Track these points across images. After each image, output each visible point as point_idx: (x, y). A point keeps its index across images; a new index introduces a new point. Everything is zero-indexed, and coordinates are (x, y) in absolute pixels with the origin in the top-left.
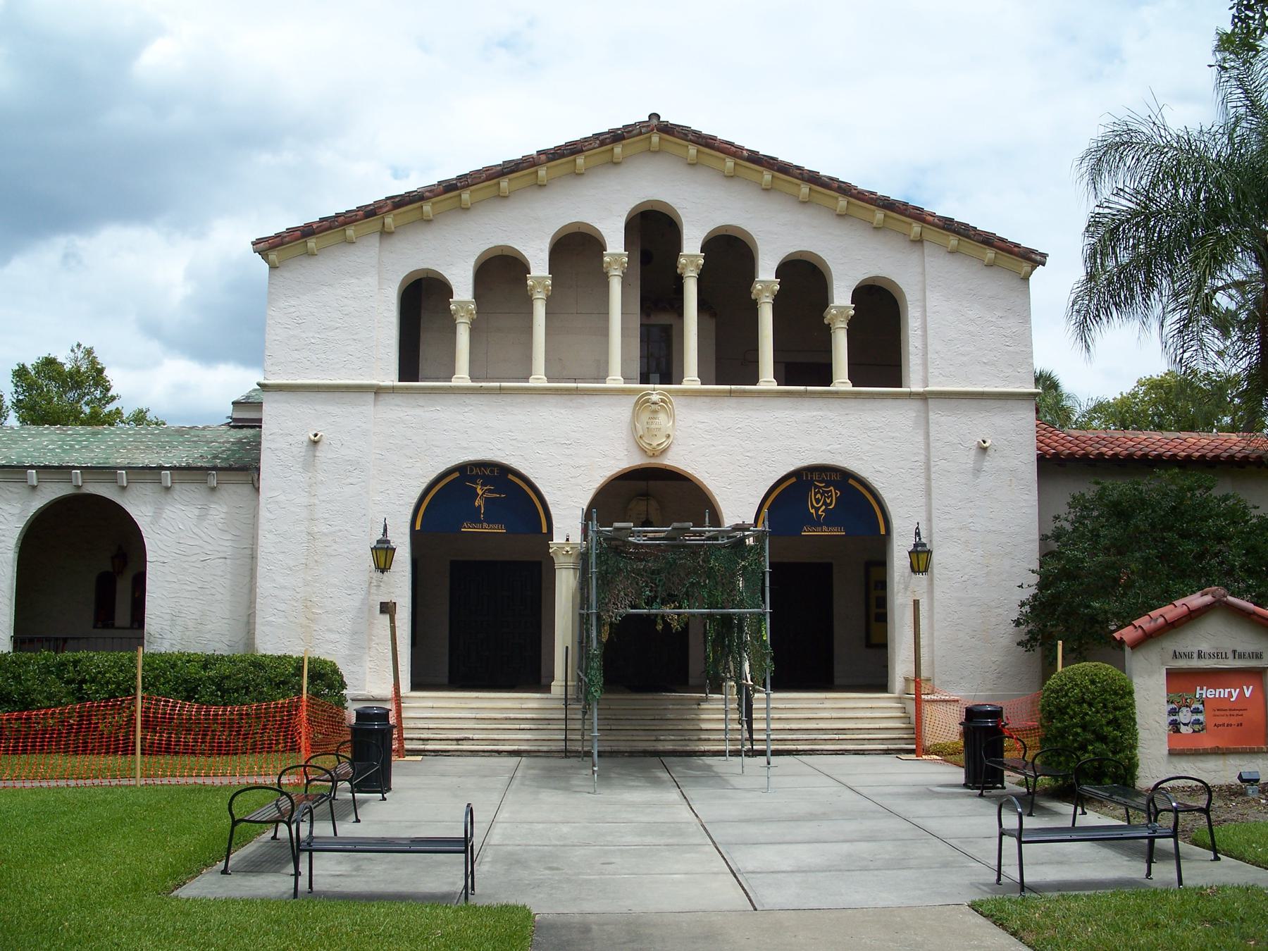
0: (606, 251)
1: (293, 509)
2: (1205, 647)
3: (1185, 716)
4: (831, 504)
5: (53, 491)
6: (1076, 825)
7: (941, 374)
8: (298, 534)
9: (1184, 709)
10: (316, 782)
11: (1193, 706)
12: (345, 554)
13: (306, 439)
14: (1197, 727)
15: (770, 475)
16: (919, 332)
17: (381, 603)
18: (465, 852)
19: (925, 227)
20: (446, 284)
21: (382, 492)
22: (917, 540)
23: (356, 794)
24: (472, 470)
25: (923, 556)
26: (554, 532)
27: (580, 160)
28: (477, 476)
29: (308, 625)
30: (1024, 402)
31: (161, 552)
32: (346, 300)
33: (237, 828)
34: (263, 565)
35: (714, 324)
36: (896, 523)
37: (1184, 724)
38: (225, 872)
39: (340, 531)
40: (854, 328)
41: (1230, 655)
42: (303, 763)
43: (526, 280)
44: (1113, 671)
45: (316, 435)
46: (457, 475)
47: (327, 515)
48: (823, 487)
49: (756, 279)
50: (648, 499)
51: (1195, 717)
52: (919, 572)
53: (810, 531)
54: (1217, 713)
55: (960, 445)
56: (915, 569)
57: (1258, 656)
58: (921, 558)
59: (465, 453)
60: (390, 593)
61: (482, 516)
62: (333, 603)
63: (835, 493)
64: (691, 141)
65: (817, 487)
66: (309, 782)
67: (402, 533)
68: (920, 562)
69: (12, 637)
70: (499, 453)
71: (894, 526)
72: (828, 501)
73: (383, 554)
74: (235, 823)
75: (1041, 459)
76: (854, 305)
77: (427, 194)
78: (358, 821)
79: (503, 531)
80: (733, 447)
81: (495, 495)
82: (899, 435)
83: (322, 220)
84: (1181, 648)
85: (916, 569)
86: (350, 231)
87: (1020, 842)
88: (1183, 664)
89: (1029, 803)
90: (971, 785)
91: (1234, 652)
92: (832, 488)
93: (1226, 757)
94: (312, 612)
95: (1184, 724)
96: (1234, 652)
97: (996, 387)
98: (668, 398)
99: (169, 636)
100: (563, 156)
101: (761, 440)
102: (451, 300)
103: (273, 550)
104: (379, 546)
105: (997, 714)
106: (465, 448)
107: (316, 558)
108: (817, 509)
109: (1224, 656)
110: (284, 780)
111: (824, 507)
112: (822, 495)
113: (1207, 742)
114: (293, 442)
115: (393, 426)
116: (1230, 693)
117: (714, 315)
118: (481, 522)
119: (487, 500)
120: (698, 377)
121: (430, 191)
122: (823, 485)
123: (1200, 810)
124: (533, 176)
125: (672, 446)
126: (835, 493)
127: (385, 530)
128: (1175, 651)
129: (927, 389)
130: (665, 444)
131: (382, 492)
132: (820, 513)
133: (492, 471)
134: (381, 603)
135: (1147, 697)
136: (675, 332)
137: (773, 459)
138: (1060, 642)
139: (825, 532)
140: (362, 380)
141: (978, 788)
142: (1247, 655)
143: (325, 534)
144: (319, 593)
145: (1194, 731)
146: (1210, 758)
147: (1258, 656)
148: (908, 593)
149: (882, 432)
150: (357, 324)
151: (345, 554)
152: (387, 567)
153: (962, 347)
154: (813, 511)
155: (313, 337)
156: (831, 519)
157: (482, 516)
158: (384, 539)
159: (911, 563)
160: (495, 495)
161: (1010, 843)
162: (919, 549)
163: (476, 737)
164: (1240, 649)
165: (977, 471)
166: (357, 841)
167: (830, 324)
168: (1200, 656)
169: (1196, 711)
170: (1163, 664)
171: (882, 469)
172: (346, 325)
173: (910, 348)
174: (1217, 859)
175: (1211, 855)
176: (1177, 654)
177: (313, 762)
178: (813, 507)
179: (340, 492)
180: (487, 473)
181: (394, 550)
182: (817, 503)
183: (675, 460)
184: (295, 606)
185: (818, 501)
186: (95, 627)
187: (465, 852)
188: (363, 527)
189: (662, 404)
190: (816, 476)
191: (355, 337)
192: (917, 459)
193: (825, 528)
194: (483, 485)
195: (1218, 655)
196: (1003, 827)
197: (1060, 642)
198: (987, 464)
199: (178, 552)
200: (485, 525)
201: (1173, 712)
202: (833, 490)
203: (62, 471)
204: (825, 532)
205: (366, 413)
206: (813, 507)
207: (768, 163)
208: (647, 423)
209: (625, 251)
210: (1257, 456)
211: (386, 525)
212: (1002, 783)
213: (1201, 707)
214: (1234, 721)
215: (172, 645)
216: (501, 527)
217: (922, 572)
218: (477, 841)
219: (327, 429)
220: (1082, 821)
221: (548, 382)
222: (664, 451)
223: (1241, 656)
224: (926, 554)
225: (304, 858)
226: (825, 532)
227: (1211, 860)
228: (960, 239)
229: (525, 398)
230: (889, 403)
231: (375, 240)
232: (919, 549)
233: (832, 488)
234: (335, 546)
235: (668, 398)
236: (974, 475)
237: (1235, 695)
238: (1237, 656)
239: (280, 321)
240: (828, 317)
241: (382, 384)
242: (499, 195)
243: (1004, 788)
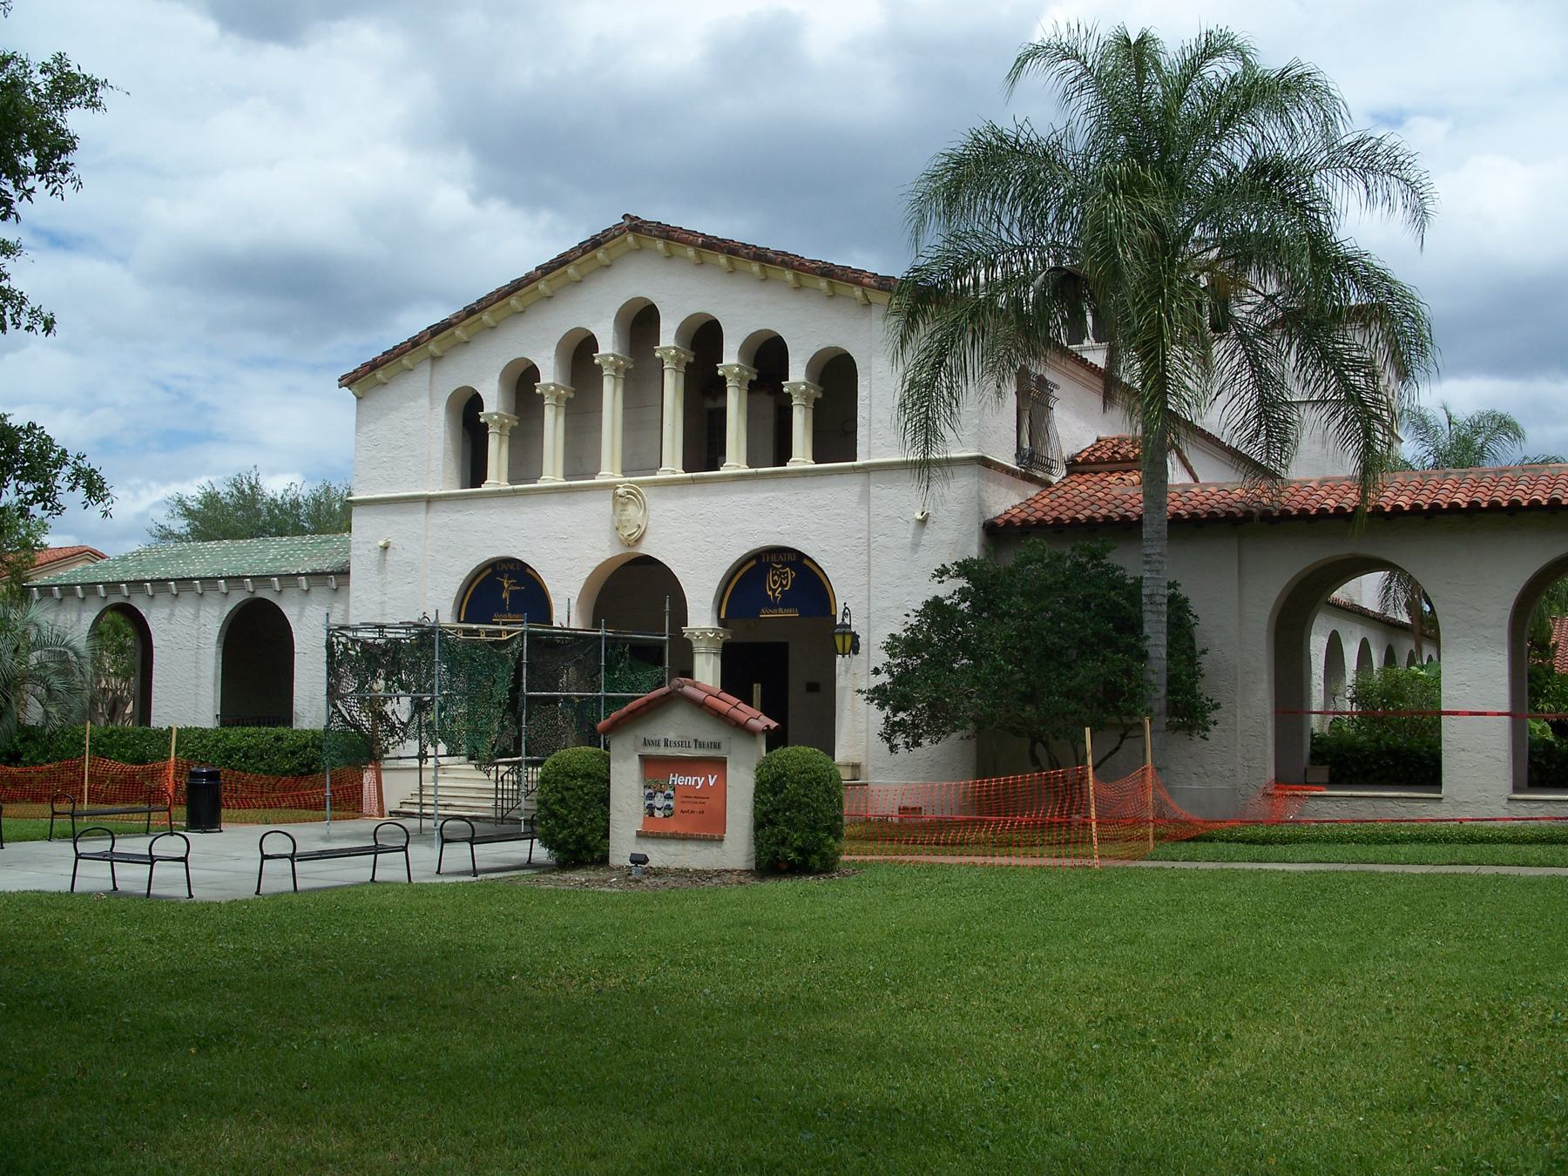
2: (671, 736)
3: (659, 801)
4: (786, 586)
5: (238, 597)
9: (659, 794)
11: (666, 792)
14: (668, 812)
16: (867, 402)
27: (571, 270)
28: (504, 572)
30: (966, 468)
31: (305, 646)
37: (659, 809)
41: (693, 744)
44: (821, 755)
46: (489, 571)
51: (667, 802)
54: (685, 800)
57: (717, 746)
63: (791, 574)
64: (655, 236)
72: (784, 583)
77: (455, 320)
83: (384, 353)
86: (405, 361)
88: (651, 751)
91: (696, 741)
93: (685, 842)
95: (659, 809)
99: (308, 715)
100: (554, 269)
106: (490, 547)
108: (774, 591)
112: (779, 576)
113: (673, 826)
116: (696, 780)
118: (506, 612)
119: (512, 593)
121: (457, 317)
125: (646, 535)
126: (791, 574)
133: (515, 566)
138: (1088, 730)
139: (781, 614)
145: (665, 816)
146: (671, 842)
147: (717, 746)
148: (849, 675)
154: (770, 593)
156: (787, 600)
163: (457, 803)
164: (701, 739)
165: (916, 546)
168: (666, 745)
169: (668, 797)
170: (635, 750)
171: (827, 548)
178: (771, 589)
185: (775, 583)
190: (774, 558)
191: (414, 453)
192: (860, 535)
193: (780, 610)
194: (509, 579)
197: (1088, 730)
198: (925, 538)
201: (650, 797)
203: (235, 580)
204: (781, 614)
205: (443, 518)
206: (771, 589)
207: (719, 246)
213: (672, 793)
214: (698, 808)
215: (310, 722)
221: (625, 476)
222: (638, 541)
229: (481, 502)
230: (835, 478)
231: (427, 367)
236: (913, 549)
237: (700, 783)
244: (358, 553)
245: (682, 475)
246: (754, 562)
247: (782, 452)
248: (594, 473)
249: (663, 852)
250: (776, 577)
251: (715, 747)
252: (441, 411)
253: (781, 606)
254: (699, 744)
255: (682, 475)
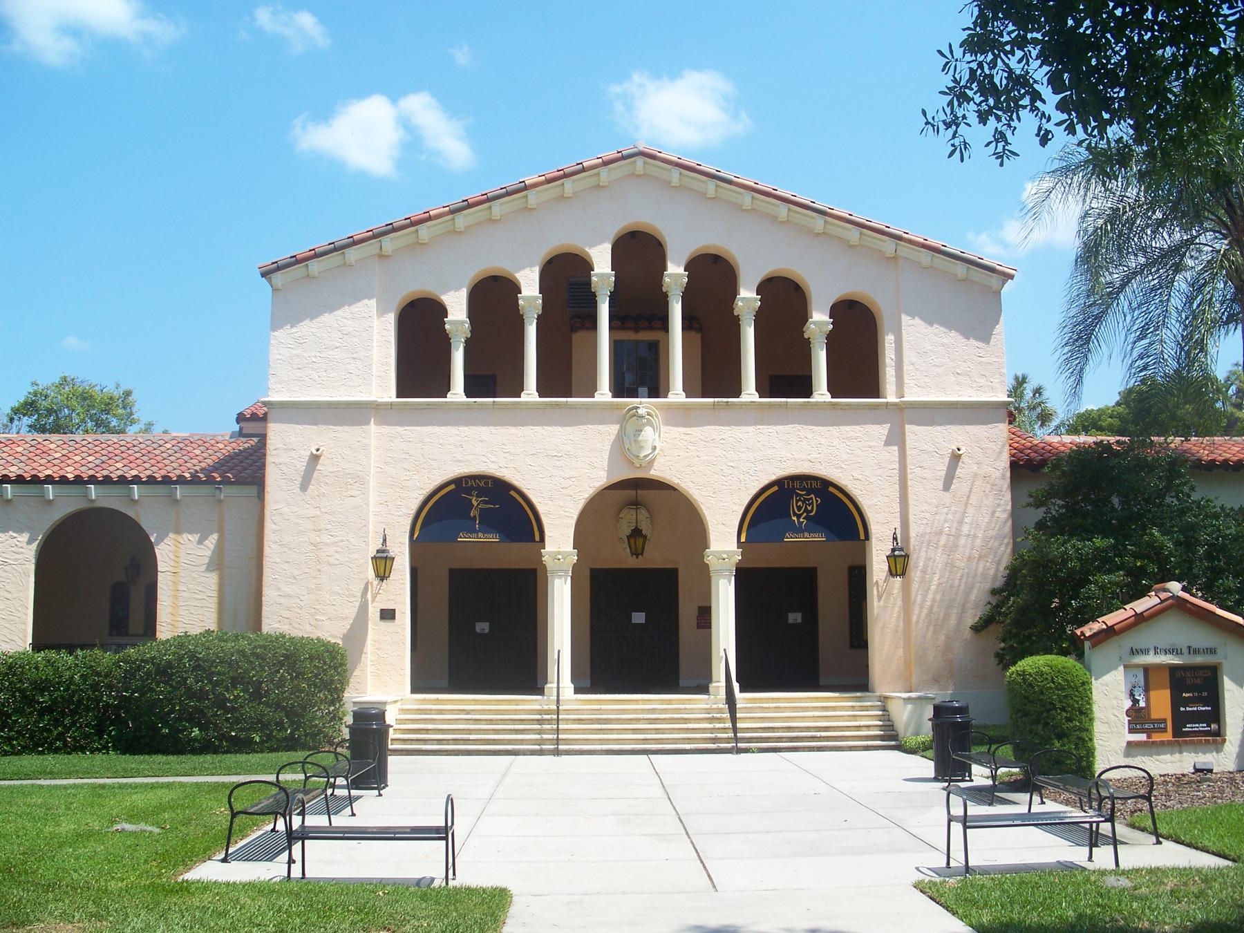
0: (593, 271)
1: (296, 521)
5: (63, 504)
6: (1032, 811)
7: (916, 385)
8: (302, 544)
10: (314, 779)
12: (346, 563)
13: (309, 453)
15: (753, 484)
17: (382, 610)
18: (446, 839)
19: (901, 245)
20: (517, 286)
21: (381, 504)
22: (895, 544)
23: (352, 791)
24: (467, 483)
25: (899, 560)
26: (546, 541)
29: (312, 631)
32: (345, 320)
33: (236, 820)
34: (269, 575)
35: (699, 341)
36: (874, 529)
38: (224, 860)
39: (342, 541)
40: (833, 341)
42: (302, 760)
43: (517, 299)
45: (318, 450)
46: (452, 487)
47: (329, 526)
48: (804, 495)
49: (738, 296)
50: (637, 508)
52: (897, 575)
53: (466, 538)
55: (935, 453)
56: (892, 573)
58: (899, 563)
59: (461, 466)
60: (389, 600)
61: (477, 526)
62: (335, 610)
63: (816, 501)
65: (798, 495)
66: (307, 778)
67: (400, 543)
68: (898, 566)
69: (30, 644)
70: (492, 465)
71: (873, 531)
72: (809, 508)
73: (383, 564)
74: (234, 815)
75: (1014, 465)
76: (832, 320)
78: (353, 815)
79: (824, 539)
80: (717, 457)
81: (489, 506)
82: (877, 444)
84: (1137, 646)
85: (894, 572)
87: (965, 828)
89: (986, 795)
90: (940, 778)
91: (1189, 647)
92: (812, 496)
94: (316, 619)
96: (1189, 647)
97: (970, 396)
98: (654, 411)
101: (744, 450)
102: (445, 319)
103: (278, 560)
104: (379, 555)
105: (962, 710)
106: (461, 461)
107: (319, 567)
109: (1179, 652)
110: (282, 777)
111: (805, 514)
112: (803, 502)
114: (296, 457)
115: (392, 441)
117: (700, 330)
118: (477, 532)
120: (684, 391)
122: (805, 492)
123: (1142, 797)
124: (524, 200)
126: (816, 501)
127: (385, 540)
128: (1132, 648)
129: (902, 399)
130: (651, 455)
131: (381, 504)
132: (801, 520)
133: (486, 483)
134: (382, 610)
135: (1106, 692)
136: (661, 345)
137: (756, 469)
140: (362, 397)
141: (946, 781)
142: (1202, 650)
143: (327, 544)
144: (322, 601)
147: (1212, 651)
149: (860, 441)
150: (356, 344)
151: (346, 563)
152: (386, 575)
153: (936, 358)
154: (795, 518)
155: (315, 357)
157: (477, 526)
158: (384, 548)
159: (889, 567)
160: (489, 506)
161: (957, 828)
162: (896, 553)
164: (1195, 645)
166: (346, 830)
167: (809, 338)
171: (860, 477)
172: (346, 344)
173: (887, 361)
174: (1159, 843)
175: (1154, 839)
176: (1134, 650)
177: (309, 760)
179: (341, 504)
180: (482, 484)
181: (393, 559)
182: (799, 511)
183: (660, 471)
184: (299, 614)
185: (799, 508)
186: (110, 635)
187: (446, 839)
188: (363, 537)
189: (648, 417)
190: (797, 484)
191: (355, 356)
193: (806, 534)
194: (478, 496)
195: (1173, 652)
196: (951, 813)
199: (188, 562)
200: (480, 534)
202: (814, 498)
206: (795, 514)
208: (634, 435)
209: (612, 271)
210: (1224, 460)
211: (385, 535)
212: (970, 776)
216: (496, 536)
217: (900, 575)
218: (459, 830)
219: (329, 444)
220: (1036, 808)
223: (1196, 651)
224: (903, 558)
225: (297, 848)
226: (480, 538)
227: (1154, 844)
228: (933, 255)
232: (896, 553)
233: (812, 496)
234: (337, 556)
235: (654, 411)
238: (1192, 652)
239: (283, 341)
240: (808, 332)
241: (380, 400)
242: (526, 207)
243: (972, 780)
244: (277, 461)
245: (394, 399)
246: (776, 488)
247: (804, 387)
248: (738, 394)
249: (1157, 760)
250: (800, 503)
251: (1211, 652)
252: (391, 320)
253: (806, 530)
254: (1192, 651)
255: (464, 399)
